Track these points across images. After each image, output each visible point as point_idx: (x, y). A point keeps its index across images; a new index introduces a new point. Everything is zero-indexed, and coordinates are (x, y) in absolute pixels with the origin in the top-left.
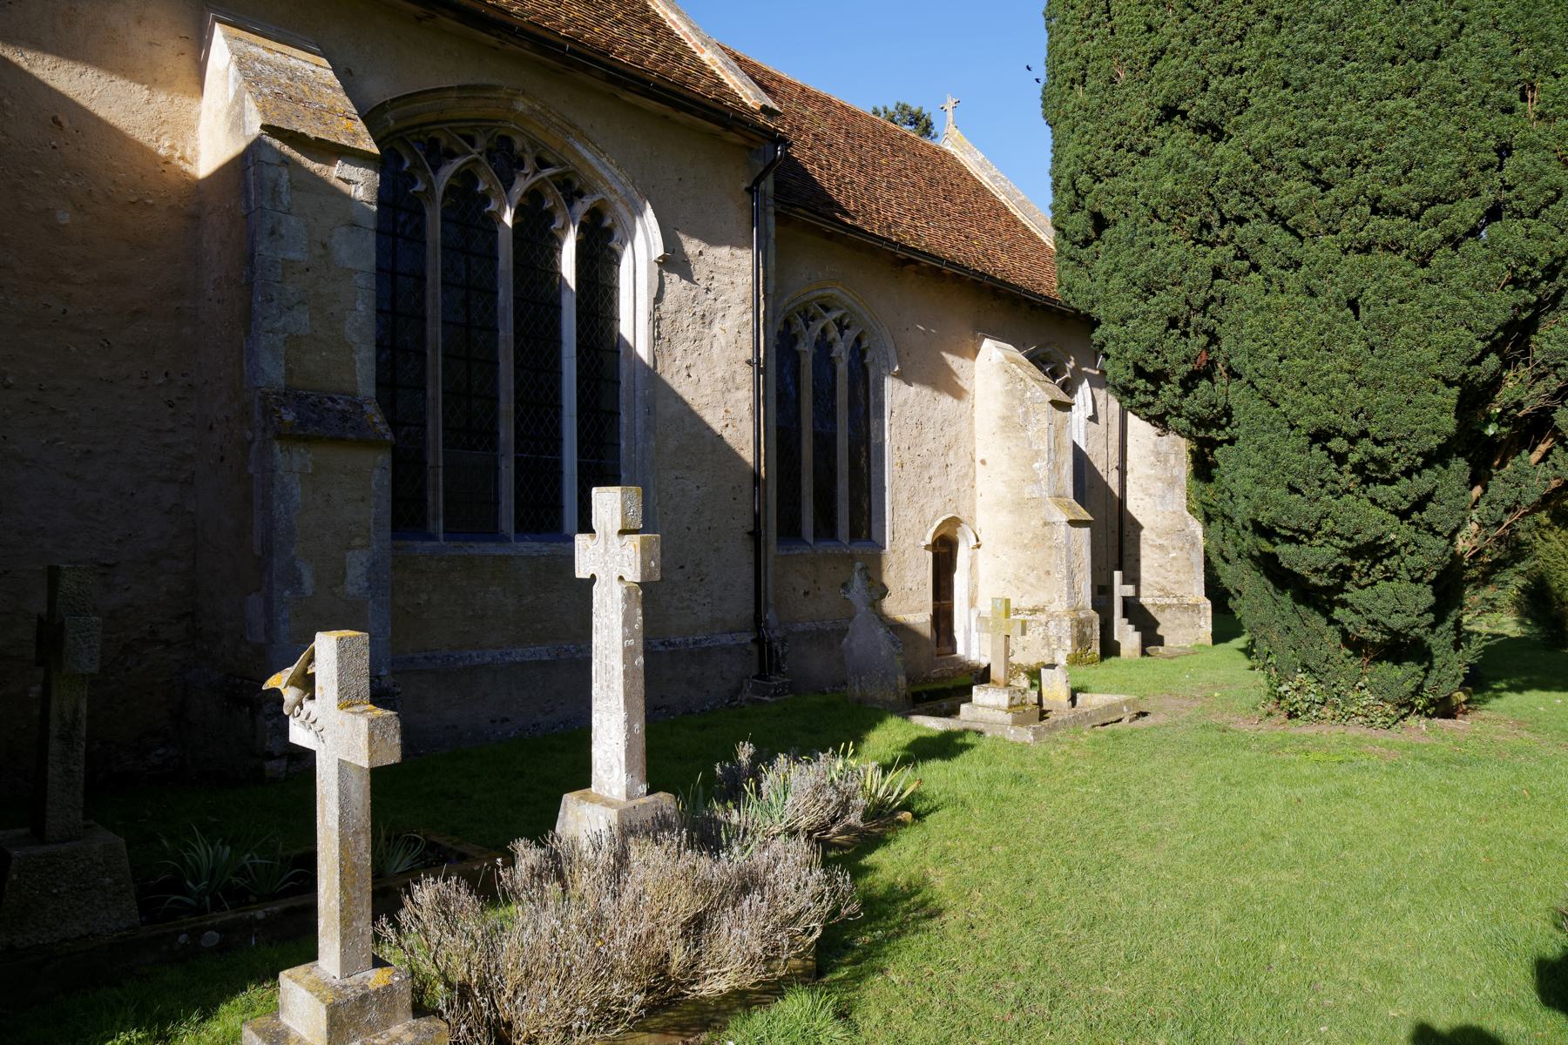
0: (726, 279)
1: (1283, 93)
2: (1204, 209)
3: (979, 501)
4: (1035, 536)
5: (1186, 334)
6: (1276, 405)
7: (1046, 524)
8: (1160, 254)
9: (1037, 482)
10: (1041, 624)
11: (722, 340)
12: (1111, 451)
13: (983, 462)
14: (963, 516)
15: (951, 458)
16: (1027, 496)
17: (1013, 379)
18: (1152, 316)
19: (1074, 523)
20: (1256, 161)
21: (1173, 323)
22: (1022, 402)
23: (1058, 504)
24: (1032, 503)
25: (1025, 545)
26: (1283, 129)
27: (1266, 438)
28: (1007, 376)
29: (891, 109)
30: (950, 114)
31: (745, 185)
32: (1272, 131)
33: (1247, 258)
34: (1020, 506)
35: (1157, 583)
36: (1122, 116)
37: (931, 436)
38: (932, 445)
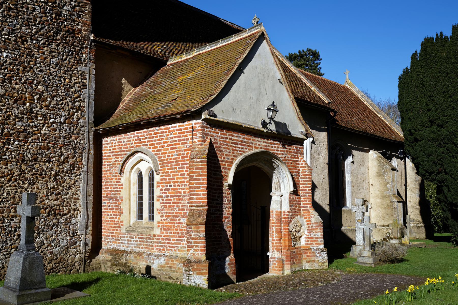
0: (322, 144)
1: (454, 122)
2: (440, 141)
3: (371, 195)
4: (388, 205)
5: (437, 165)
6: (456, 180)
7: (391, 202)
8: (431, 149)
9: (388, 190)
10: (391, 229)
11: (322, 158)
12: (403, 180)
13: (372, 185)
14: (367, 200)
15: (364, 184)
16: (385, 194)
17: (380, 162)
18: (430, 161)
19: (398, 202)
20: (450, 134)
21: (434, 162)
22: (383, 169)
23: (394, 196)
24: (387, 196)
25: (385, 208)
26: (455, 129)
27: (454, 187)
28: (378, 161)
29: (305, 50)
30: (347, 76)
31: (325, 121)
32: (453, 129)
33: (449, 150)
34: (383, 197)
35: (417, 219)
36: (421, 120)
37: (360, 178)
38: (360, 181)
